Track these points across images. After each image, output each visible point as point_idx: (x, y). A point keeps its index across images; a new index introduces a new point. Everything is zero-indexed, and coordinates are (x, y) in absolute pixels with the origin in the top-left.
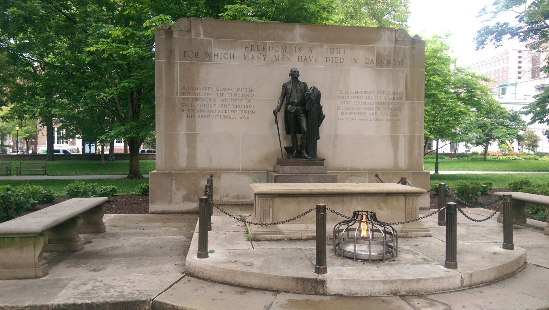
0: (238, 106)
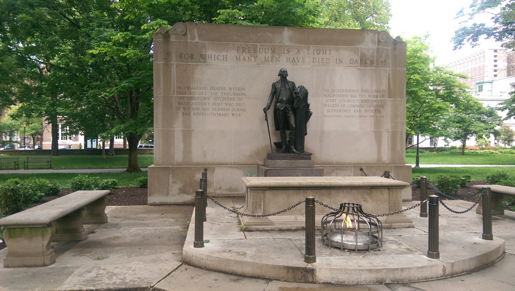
0: (230, 105)
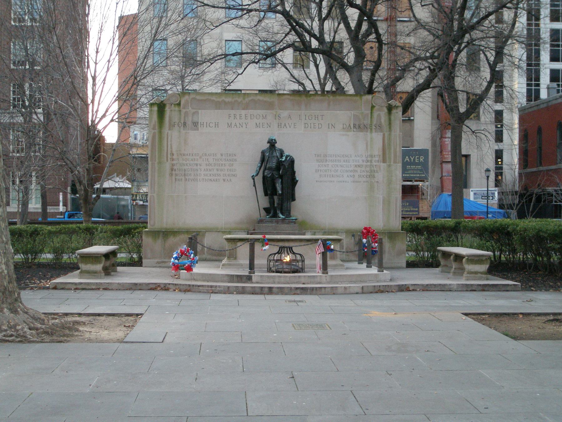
0: (222, 170)
